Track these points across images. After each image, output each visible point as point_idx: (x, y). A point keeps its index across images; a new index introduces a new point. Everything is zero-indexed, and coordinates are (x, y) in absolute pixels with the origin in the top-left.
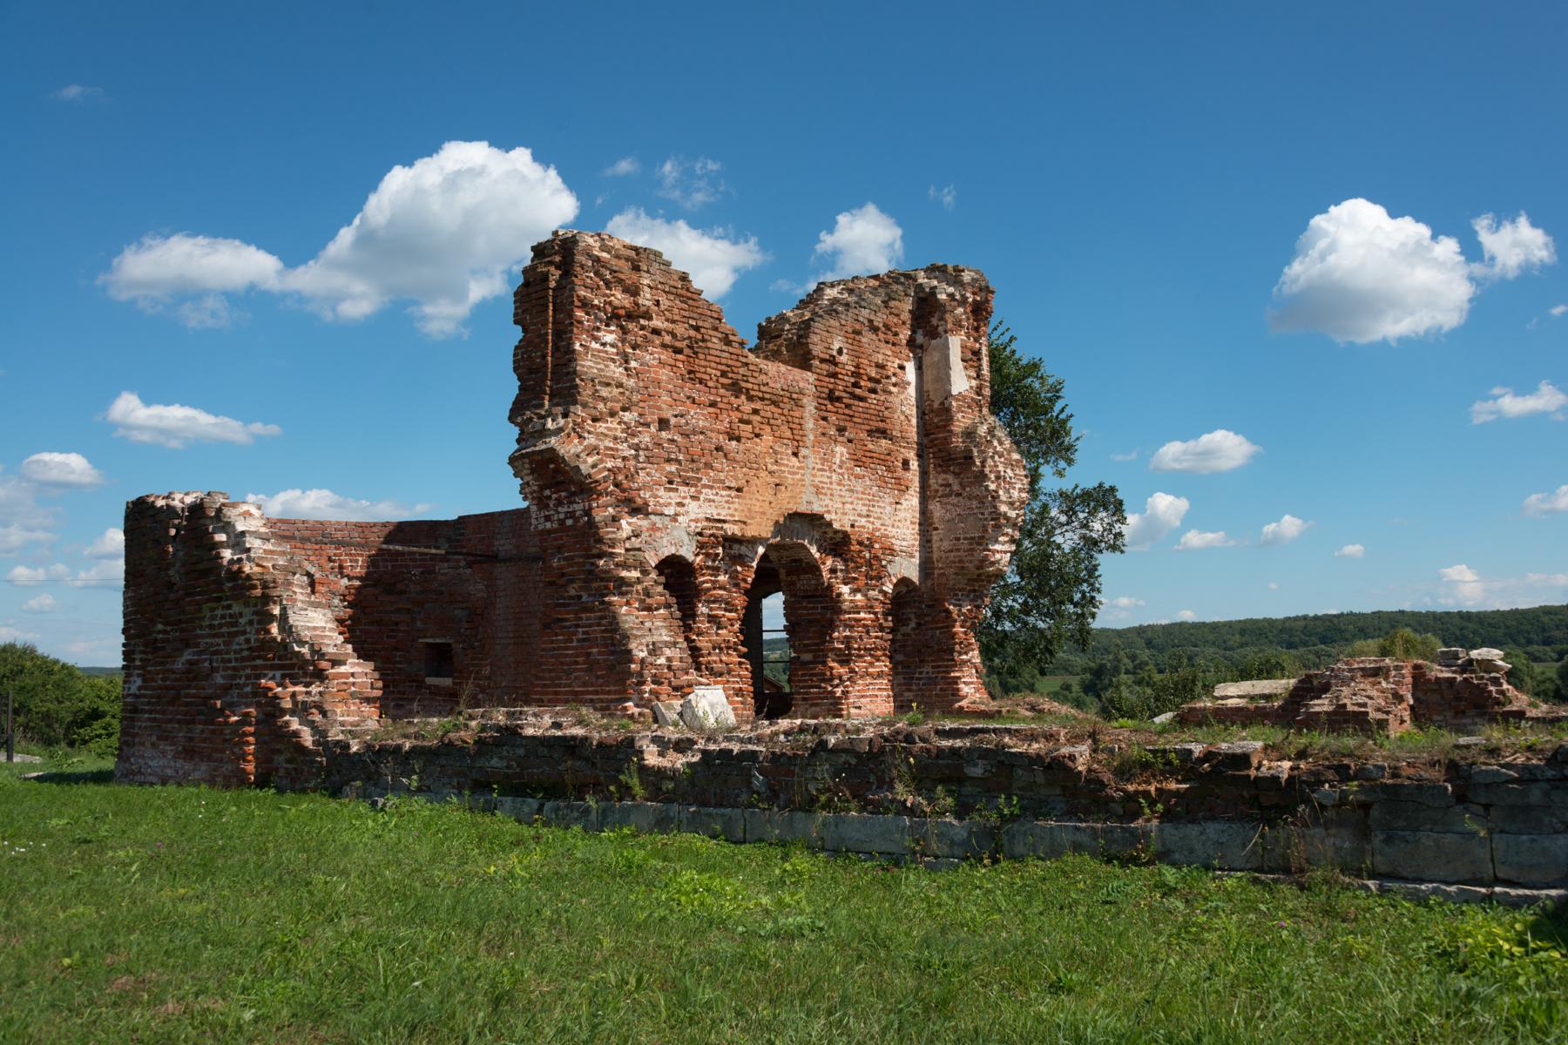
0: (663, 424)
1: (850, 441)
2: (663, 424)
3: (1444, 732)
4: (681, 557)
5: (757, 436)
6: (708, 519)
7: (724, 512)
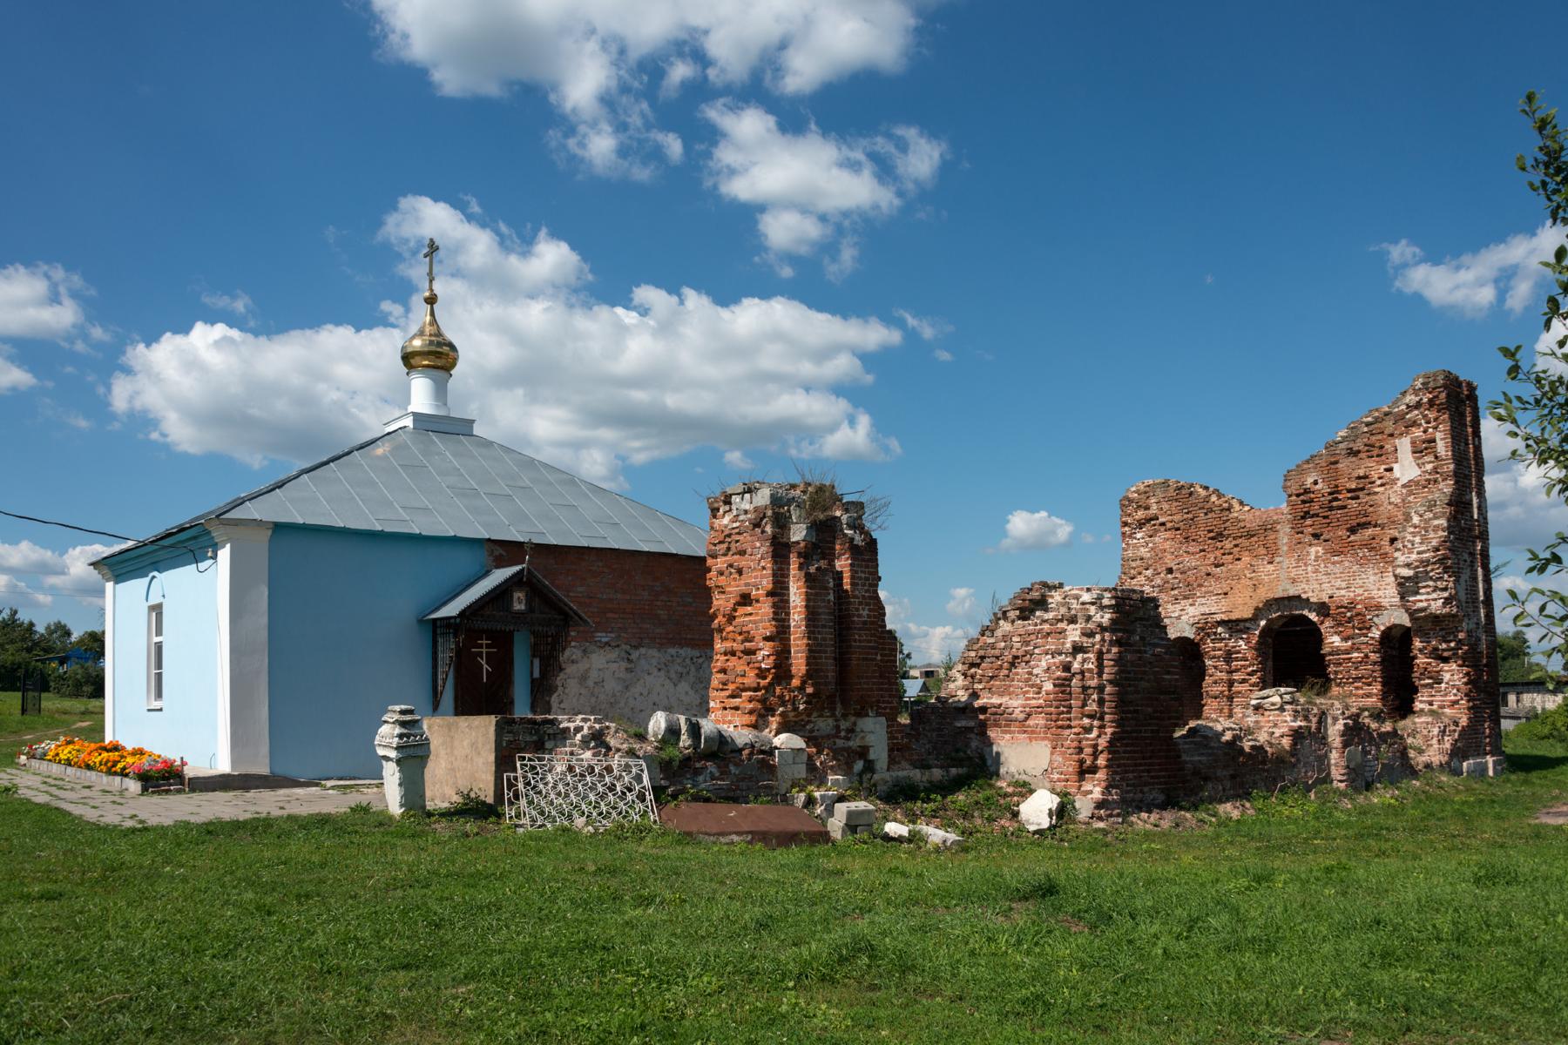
0: (1170, 571)
2: (1170, 571)
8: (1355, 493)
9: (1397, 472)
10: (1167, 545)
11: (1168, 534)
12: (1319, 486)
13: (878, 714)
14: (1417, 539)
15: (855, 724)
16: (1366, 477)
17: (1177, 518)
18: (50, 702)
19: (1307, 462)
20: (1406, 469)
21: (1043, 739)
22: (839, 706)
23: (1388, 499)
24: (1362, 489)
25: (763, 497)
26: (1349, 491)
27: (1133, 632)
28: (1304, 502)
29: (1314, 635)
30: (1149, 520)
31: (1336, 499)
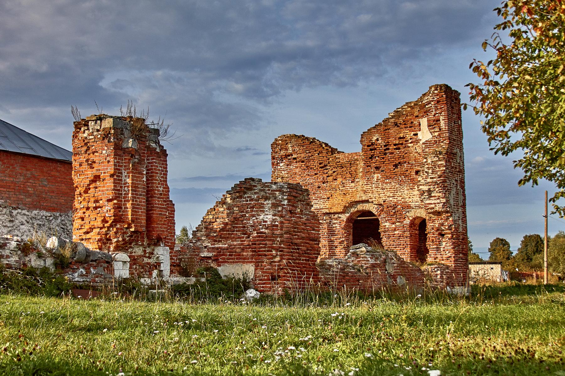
5: (336, 179)
7: (322, 206)
9: (420, 136)
11: (298, 164)
12: (380, 142)
13: (166, 245)
14: (430, 171)
15: (153, 250)
17: (303, 155)
18: (270, 99)
20: (425, 135)
21: (251, 262)
22: (145, 239)
23: (415, 149)
25: (108, 123)
26: (395, 145)
27: (296, 207)
28: (371, 150)
29: (376, 223)
30: (287, 156)
31: (388, 149)
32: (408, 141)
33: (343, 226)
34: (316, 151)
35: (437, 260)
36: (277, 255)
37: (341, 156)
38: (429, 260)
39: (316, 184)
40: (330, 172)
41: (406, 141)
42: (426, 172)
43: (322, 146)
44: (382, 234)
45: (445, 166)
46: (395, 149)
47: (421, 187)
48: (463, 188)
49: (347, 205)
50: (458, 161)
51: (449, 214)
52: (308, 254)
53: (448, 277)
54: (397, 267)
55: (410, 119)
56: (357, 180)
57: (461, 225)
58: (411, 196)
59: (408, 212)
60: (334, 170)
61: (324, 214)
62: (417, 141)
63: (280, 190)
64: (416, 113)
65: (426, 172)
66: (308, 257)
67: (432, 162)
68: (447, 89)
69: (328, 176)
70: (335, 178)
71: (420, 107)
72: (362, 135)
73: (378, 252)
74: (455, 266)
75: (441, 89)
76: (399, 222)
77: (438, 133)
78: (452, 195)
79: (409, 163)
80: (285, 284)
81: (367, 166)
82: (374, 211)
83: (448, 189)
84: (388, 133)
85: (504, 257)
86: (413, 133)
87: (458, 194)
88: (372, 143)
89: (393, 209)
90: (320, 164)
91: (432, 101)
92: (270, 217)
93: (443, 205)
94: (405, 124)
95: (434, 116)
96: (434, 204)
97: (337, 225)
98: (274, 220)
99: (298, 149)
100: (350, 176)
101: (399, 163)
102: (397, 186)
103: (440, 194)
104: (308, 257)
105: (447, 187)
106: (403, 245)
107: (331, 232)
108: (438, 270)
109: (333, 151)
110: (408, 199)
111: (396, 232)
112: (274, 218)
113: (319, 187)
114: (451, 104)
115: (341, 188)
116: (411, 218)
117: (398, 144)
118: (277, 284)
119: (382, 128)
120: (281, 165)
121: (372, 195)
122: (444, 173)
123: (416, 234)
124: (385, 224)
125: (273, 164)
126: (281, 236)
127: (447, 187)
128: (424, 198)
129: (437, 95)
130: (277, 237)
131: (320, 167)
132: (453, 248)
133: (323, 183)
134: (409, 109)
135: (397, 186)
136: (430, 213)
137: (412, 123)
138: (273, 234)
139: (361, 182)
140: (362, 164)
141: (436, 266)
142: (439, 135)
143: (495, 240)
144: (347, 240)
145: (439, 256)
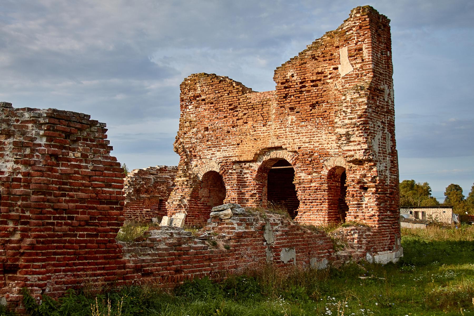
0: (207, 129)
1: (297, 112)
2: (207, 129)
3: (299, 198)
4: (215, 171)
5: (246, 123)
6: (224, 157)
7: (231, 154)
8: (315, 83)
10: (206, 113)
11: (207, 107)
12: (294, 78)
14: (349, 111)
16: (322, 73)
17: (212, 96)
19: (289, 62)
20: (346, 67)
23: (334, 86)
24: (320, 80)
26: (312, 81)
28: (285, 88)
30: (195, 97)
31: (305, 86)
32: (327, 76)
33: (254, 176)
34: (225, 91)
35: (358, 219)
36: (15, 230)
37: (252, 96)
38: (349, 218)
39: (226, 129)
40: (241, 114)
41: (325, 77)
42: (344, 111)
43: (232, 84)
44: (297, 186)
45: (366, 104)
46: (312, 86)
47: (337, 130)
48: (392, 132)
49: (258, 152)
50: (386, 100)
51: (372, 164)
52: (94, 224)
53: (369, 242)
54: (282, 235)
55: (330, 51)
56: (269, 123)
57: (389, 176)
58: (326, 141)
59: (327, 160)
60: (246, 112)
61: (233, 162)
62: (337, 76)
63: (35, 121)
64: (336, 44)
65: (344, 111)
66: (95, 230)
67: (352, 99)
68: (372, 13)
69: (238, 119)
70: (245, 121)
71: (342, 35)
72: (275, 71)
73: (253, 215)
74: (379, 227)
75: (363, 11)
76: (316, 172)
77: (360, 65)
78: (376, 138)
79: (327, 102)
80: (26, 279)
81: (281, 107)
82: (289, 160)
83: (370, 133)
84: (305, 68)
85: (457, 200)
86: (333, 67)
87: (385, 139)
88: (286, 80)
89: (309, 157)
90: (230, 105)
91: (354, 27)
92: (10, 165)
93: (364, 152)
94: (324, 57)
95: (356, 44)
96: (354, 150)
97: (248, 175)
98: (15, 170)
99: (207, 89)
100: (262, 119)
101: (317, 102)
102: (314, 130)
103: (361, 139)
104: (95, 230)
105: (369, 129)
106: (321, 199)
107: (241, 183)
108: (355, 233)
109: (244, 90)
110: (326, 145)
111: (313, 185)
112: (16, 166)
113: (229, 132)
114: (376, 31)
115: (252, 133)
116: (329, 168)
117: (315, 81)
118: (14, 280)
119: (298, 62)
120: (190, 107)
121: (285, 141)
122: (365, 112)
123: (337, 187)
124: (301, 175)
125: (182, 106)
126: (25, 197)
127: (369, 129)
128: (342, 144)
129: (360, 19)
130: (18, 200)
131: (230, 109)
132: (377, 205)
133: (233, 127)
134: (329, 38)
135: (314, 130)
136: (350, 162)
137: (332, 55)
138: (9, 193)
139: (273, 125)
140: (275, 105)
141: (353, 228)
142: (362, 67)
143: (450, 186)
144: (259, 192)
145: (360, 214)
